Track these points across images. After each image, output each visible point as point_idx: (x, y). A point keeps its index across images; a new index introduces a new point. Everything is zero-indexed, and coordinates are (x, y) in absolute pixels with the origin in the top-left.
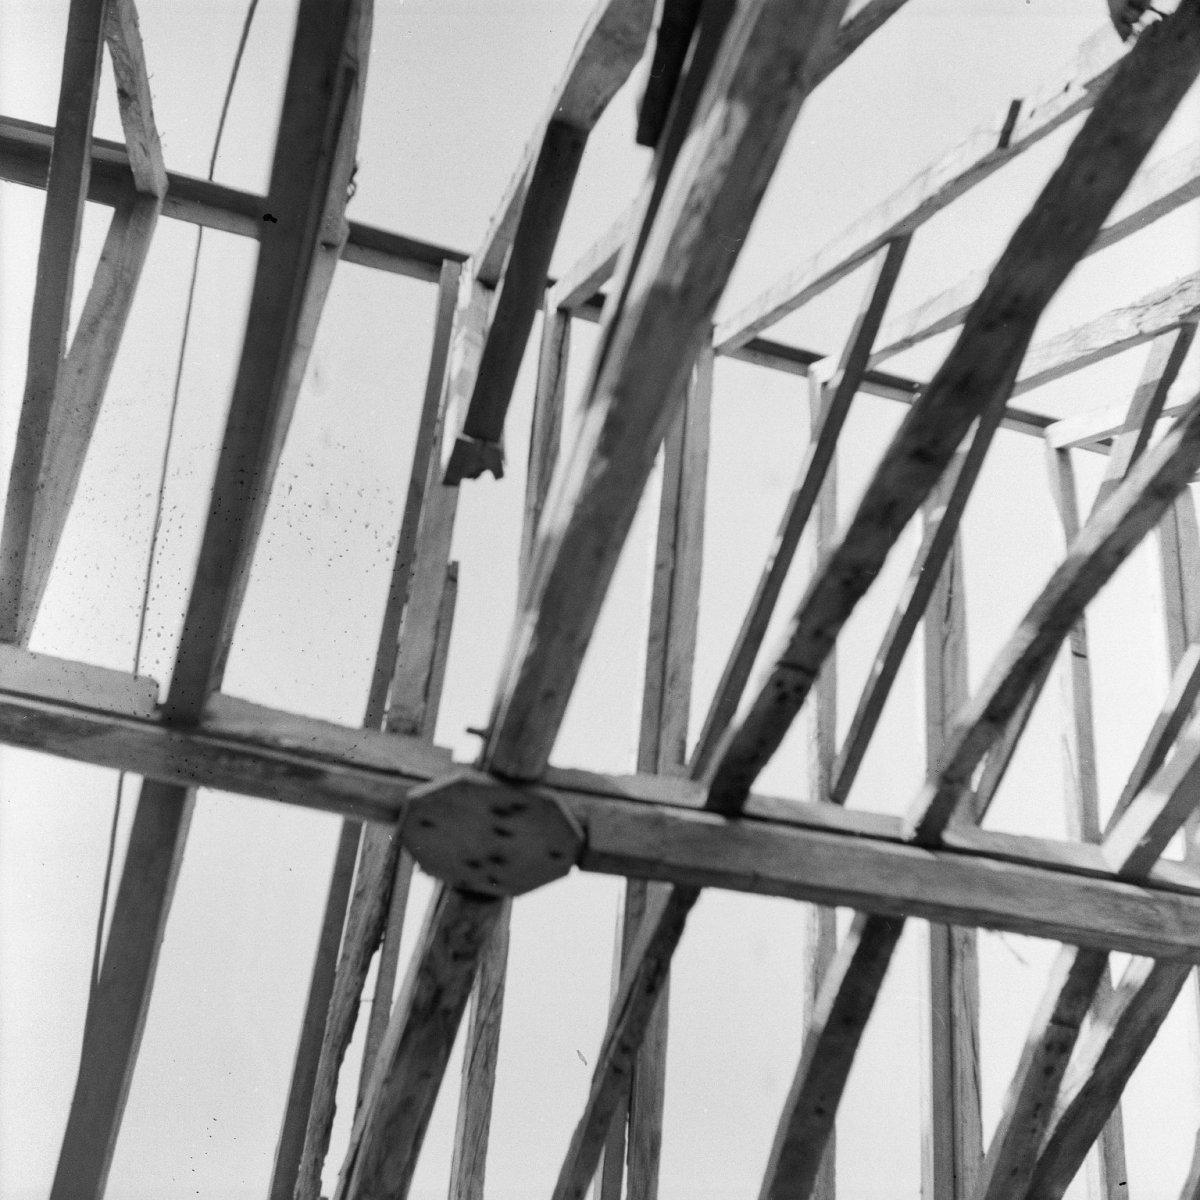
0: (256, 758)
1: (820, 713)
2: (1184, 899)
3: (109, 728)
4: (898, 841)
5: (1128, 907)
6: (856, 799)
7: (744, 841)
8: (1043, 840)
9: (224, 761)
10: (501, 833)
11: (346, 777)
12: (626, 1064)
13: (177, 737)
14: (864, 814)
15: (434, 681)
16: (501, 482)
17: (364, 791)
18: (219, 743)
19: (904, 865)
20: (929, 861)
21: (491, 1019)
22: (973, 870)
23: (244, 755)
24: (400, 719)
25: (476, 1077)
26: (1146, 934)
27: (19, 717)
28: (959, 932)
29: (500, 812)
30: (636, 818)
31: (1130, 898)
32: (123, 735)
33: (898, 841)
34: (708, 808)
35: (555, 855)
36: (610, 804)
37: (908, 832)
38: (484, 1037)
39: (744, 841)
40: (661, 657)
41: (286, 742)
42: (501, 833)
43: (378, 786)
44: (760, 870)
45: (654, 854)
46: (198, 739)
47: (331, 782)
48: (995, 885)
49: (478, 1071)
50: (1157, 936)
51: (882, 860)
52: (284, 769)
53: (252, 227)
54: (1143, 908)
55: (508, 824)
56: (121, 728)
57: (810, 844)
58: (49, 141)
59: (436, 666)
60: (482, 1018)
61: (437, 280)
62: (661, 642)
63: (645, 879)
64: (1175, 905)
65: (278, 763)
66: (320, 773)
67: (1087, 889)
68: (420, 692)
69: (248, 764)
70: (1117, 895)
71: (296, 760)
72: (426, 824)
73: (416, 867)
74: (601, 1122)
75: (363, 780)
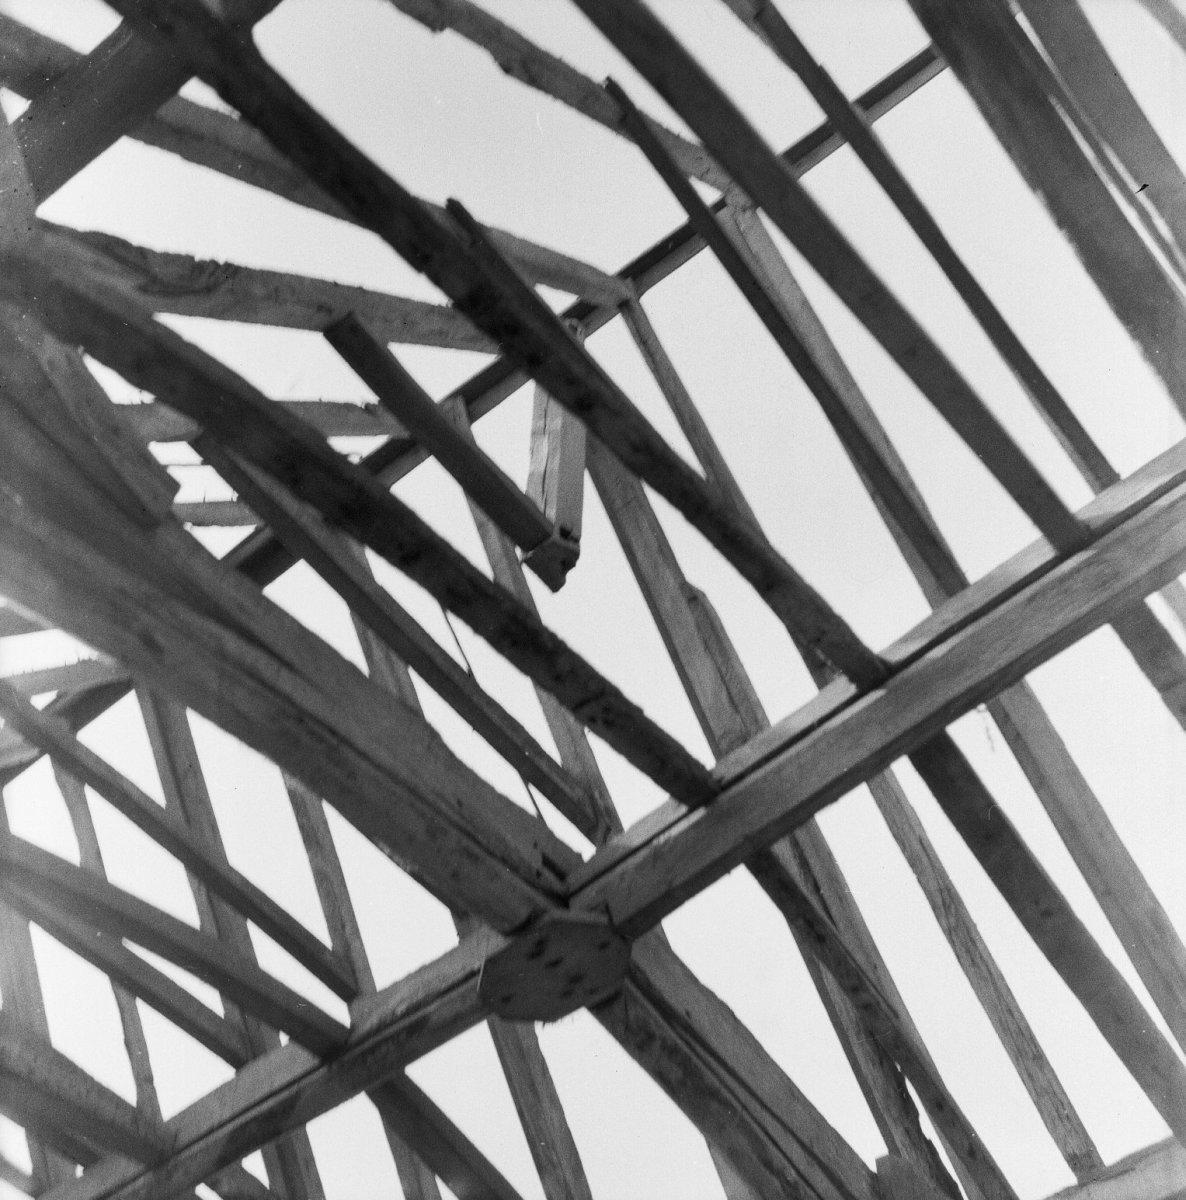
0: (386, 1040)
5: (1077, 584)
6: (1124, 462)
8: (990, 574)
10: (555, 963)
12: (864, 996)
14: (643, 822)
17: (458, 1007)
20: (882, 697)
22: (919, 674)
23: (378, 1045)
26: (1104, 596)
28: (1004, 697)
30: (640, 867)
31: (1077, 570)
34: (691, 811)
37: (1048, 553)
42: (555, 963)
43: (463, 997)
44: (747, 830)
45: (663, 888)
50: (1118, 586)
53: (520, 376)
54: (1094, 570)
55: (551, 954)
57: (779, 770)
58: (268, 533)
63: (792, 832)
66: (425, 1020)
67: (1031, 599)
70: (1062, 579)
73: (538, 1026)
74: (898, 1048)
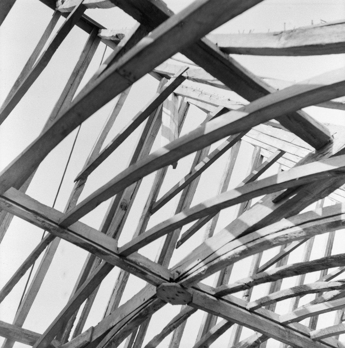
0: (135, 268)
1: (212, 224)
2: (291, 331)
3: (107, 254)
4: (245, 309)
5: (281, 331)
7: (219, 305)
9: (129, 267)
11: (151, 276)
13: (121, 260)
15: (134, 195)
16: (174, 169)
18: (128, 262)
19: (245, 315)
21: (125, 281)
24: (124, 203)
25: (119, 293)
27: (92, 248)
29: (179, 292)
31: (282, 329)
32: (111, 257)
33: (245, 309)
35: (185, 301)
36: (197, 291)
38: (123, 285)
39: (219, 305)
40: (183, 200)
41: (141, 264)
43: (157, 279)
46: (125, 261)
47: (148, 276)
48: (260, 323)
49: (119, 292)
51: (242, 314)
52: (142, 272)
55: (179, 294)
56: (111, 255)
57: (230, 308)
59: (135, 191)
60: (123, 280)
61: (160, 80)
62: (184, 197)
64: (289, 332)
65: (139, 270)
66: (146, 274)
67: (275, 326)
68: (130, 197)
69: (133, 269)
70: (280, 328)
71: (143, 270)
72: (163, 290)
75: (154, 277)
